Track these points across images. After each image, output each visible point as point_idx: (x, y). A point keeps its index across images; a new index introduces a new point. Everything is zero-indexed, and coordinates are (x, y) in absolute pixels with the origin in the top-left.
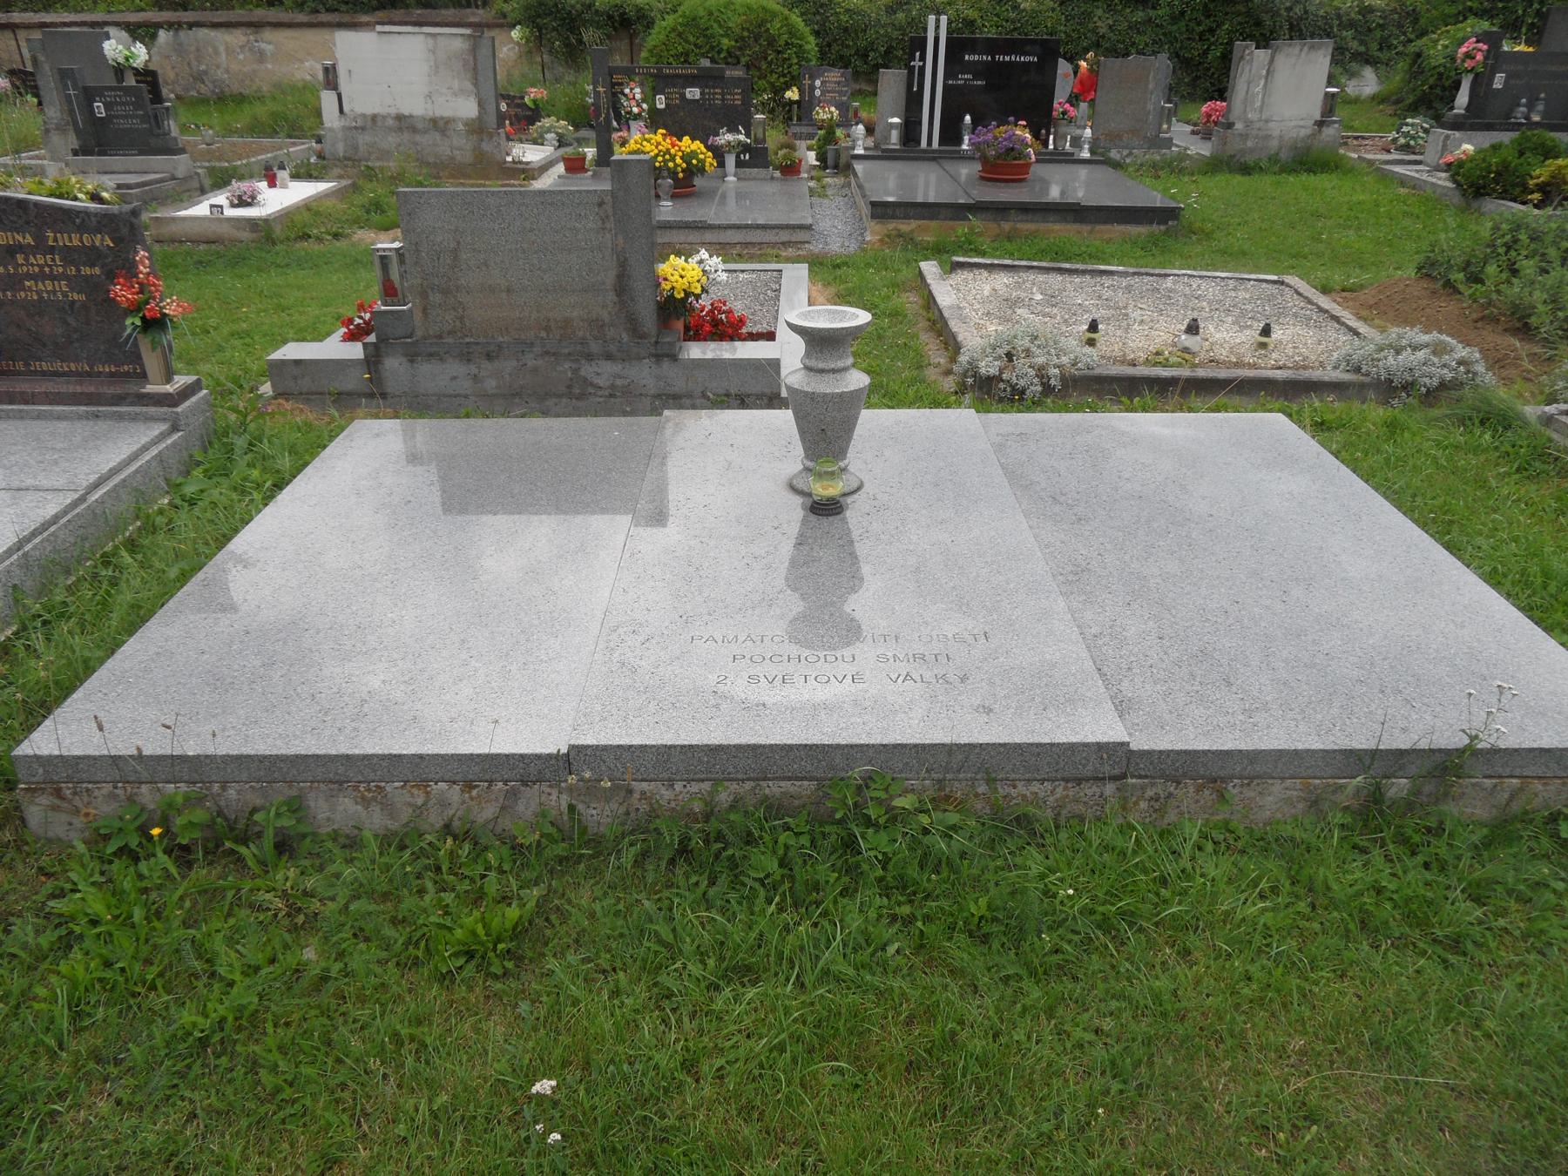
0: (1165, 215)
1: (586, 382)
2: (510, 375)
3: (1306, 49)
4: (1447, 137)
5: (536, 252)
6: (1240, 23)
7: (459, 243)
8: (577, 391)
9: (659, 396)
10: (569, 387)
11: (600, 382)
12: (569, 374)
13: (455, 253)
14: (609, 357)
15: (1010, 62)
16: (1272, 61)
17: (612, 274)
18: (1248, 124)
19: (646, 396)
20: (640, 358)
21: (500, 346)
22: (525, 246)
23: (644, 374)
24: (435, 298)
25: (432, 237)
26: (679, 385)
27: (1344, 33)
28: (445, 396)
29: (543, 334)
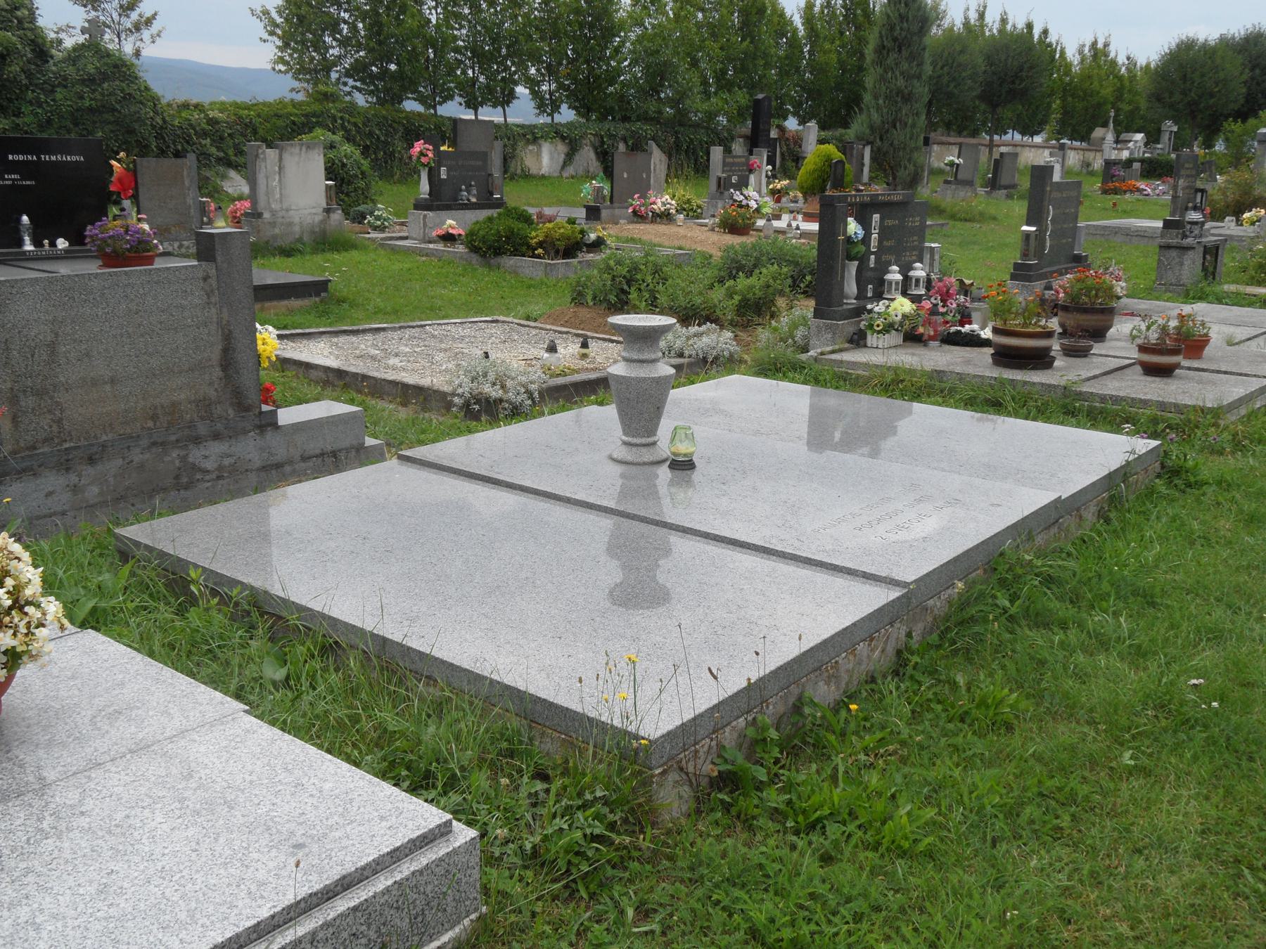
0: (319, 288)
1: (195, 468)
2: (115, 476)
3: (304, 149)
4: (425, 216)
5: (142, 336)
6: (112, 131)
7: (57, 335)
8: (185, 480)
9: (264, 468)
10: (177, 477)
11: (209, 465)
12: (177, 463)
13: (52, 347)
14: (216, 436)
15: (57, 162)
16: (281, 159)
17: (218, 348)
18: (273, 213)
19: (251, 471)
20: (245, 432)
21: (104, 446)
22: (130, 330)
23: (249, 449)
24: (28, 402)
25: (25, 332)
26: (281, 454)
27: (204, 142)
28: (38, 518)
29: (150, 424)
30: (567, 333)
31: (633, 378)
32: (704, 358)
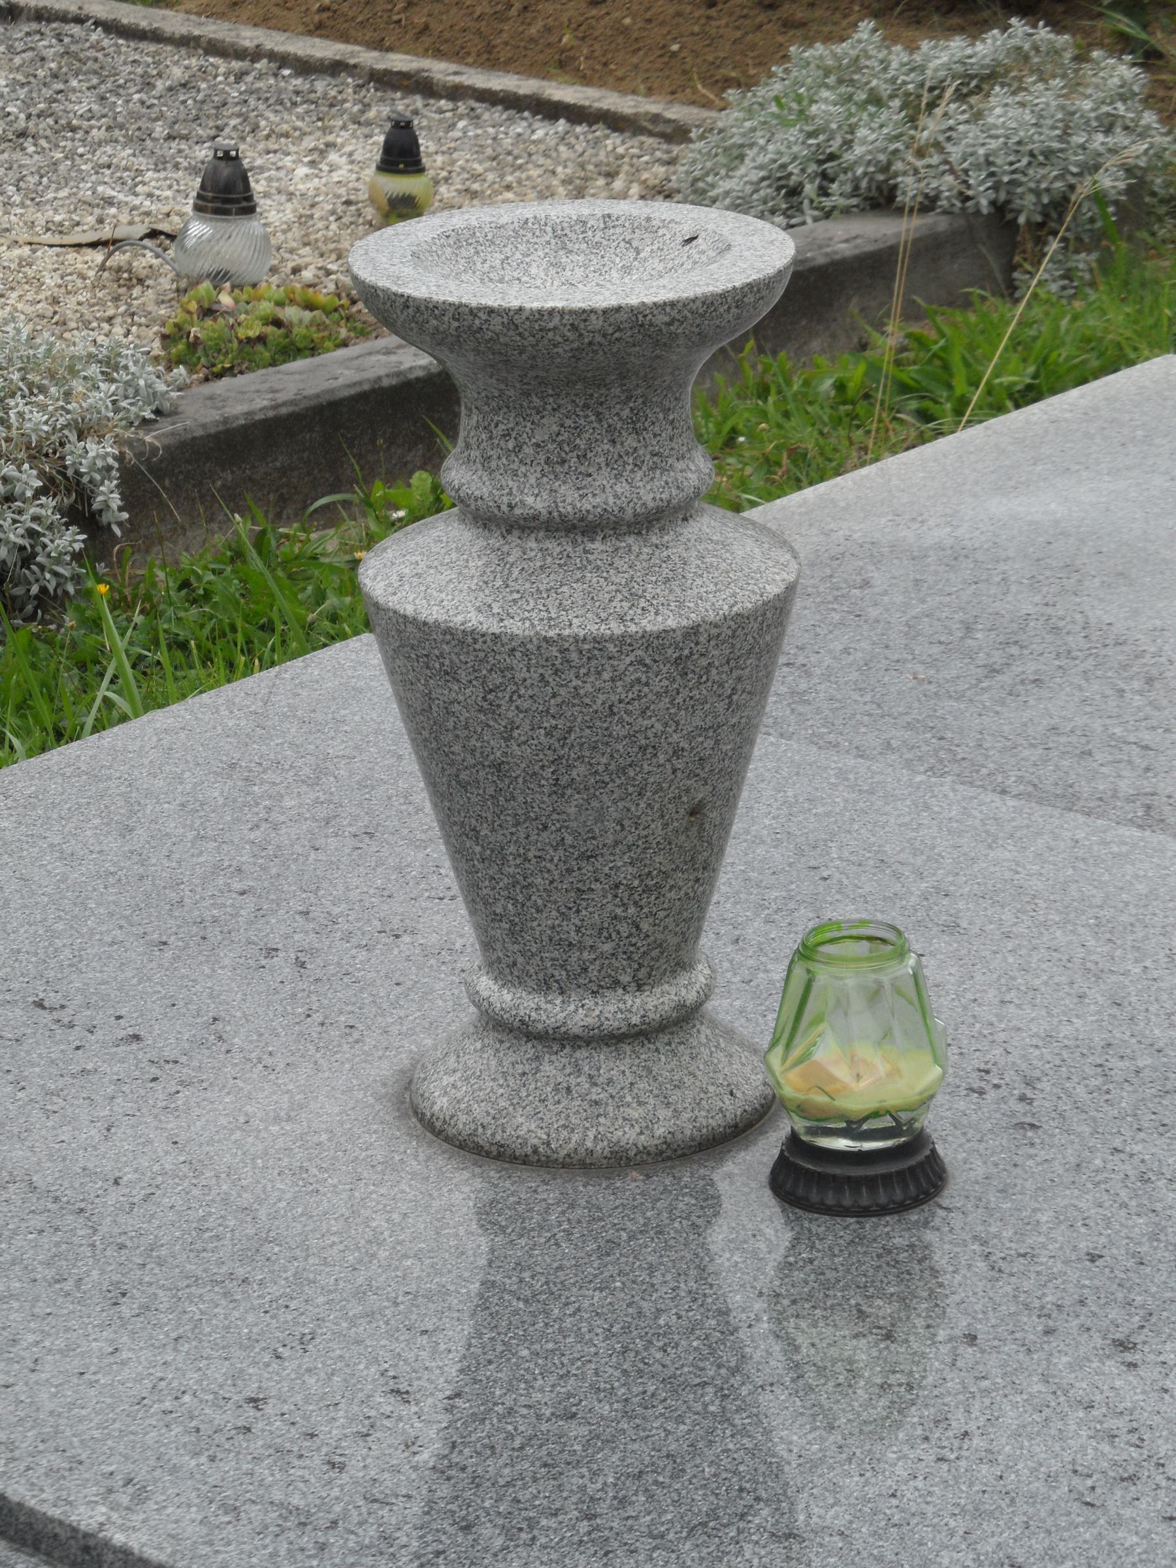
30: (335, 68)
31: (521, 647)
32: (1000, 209)
